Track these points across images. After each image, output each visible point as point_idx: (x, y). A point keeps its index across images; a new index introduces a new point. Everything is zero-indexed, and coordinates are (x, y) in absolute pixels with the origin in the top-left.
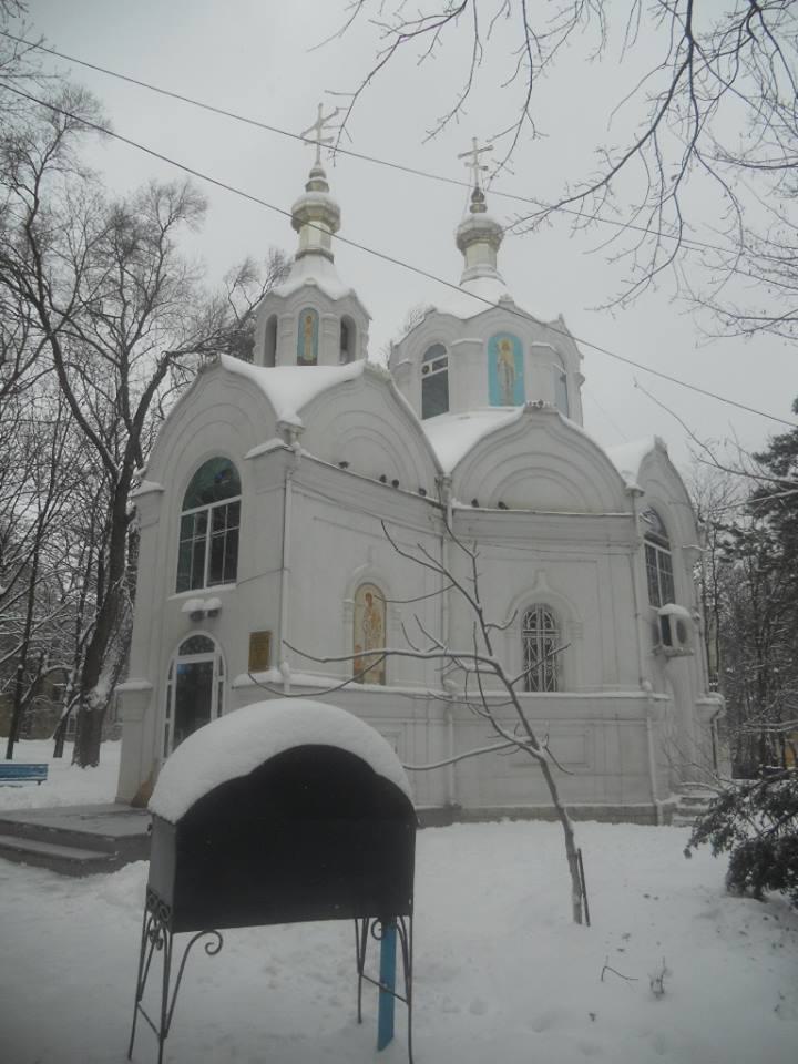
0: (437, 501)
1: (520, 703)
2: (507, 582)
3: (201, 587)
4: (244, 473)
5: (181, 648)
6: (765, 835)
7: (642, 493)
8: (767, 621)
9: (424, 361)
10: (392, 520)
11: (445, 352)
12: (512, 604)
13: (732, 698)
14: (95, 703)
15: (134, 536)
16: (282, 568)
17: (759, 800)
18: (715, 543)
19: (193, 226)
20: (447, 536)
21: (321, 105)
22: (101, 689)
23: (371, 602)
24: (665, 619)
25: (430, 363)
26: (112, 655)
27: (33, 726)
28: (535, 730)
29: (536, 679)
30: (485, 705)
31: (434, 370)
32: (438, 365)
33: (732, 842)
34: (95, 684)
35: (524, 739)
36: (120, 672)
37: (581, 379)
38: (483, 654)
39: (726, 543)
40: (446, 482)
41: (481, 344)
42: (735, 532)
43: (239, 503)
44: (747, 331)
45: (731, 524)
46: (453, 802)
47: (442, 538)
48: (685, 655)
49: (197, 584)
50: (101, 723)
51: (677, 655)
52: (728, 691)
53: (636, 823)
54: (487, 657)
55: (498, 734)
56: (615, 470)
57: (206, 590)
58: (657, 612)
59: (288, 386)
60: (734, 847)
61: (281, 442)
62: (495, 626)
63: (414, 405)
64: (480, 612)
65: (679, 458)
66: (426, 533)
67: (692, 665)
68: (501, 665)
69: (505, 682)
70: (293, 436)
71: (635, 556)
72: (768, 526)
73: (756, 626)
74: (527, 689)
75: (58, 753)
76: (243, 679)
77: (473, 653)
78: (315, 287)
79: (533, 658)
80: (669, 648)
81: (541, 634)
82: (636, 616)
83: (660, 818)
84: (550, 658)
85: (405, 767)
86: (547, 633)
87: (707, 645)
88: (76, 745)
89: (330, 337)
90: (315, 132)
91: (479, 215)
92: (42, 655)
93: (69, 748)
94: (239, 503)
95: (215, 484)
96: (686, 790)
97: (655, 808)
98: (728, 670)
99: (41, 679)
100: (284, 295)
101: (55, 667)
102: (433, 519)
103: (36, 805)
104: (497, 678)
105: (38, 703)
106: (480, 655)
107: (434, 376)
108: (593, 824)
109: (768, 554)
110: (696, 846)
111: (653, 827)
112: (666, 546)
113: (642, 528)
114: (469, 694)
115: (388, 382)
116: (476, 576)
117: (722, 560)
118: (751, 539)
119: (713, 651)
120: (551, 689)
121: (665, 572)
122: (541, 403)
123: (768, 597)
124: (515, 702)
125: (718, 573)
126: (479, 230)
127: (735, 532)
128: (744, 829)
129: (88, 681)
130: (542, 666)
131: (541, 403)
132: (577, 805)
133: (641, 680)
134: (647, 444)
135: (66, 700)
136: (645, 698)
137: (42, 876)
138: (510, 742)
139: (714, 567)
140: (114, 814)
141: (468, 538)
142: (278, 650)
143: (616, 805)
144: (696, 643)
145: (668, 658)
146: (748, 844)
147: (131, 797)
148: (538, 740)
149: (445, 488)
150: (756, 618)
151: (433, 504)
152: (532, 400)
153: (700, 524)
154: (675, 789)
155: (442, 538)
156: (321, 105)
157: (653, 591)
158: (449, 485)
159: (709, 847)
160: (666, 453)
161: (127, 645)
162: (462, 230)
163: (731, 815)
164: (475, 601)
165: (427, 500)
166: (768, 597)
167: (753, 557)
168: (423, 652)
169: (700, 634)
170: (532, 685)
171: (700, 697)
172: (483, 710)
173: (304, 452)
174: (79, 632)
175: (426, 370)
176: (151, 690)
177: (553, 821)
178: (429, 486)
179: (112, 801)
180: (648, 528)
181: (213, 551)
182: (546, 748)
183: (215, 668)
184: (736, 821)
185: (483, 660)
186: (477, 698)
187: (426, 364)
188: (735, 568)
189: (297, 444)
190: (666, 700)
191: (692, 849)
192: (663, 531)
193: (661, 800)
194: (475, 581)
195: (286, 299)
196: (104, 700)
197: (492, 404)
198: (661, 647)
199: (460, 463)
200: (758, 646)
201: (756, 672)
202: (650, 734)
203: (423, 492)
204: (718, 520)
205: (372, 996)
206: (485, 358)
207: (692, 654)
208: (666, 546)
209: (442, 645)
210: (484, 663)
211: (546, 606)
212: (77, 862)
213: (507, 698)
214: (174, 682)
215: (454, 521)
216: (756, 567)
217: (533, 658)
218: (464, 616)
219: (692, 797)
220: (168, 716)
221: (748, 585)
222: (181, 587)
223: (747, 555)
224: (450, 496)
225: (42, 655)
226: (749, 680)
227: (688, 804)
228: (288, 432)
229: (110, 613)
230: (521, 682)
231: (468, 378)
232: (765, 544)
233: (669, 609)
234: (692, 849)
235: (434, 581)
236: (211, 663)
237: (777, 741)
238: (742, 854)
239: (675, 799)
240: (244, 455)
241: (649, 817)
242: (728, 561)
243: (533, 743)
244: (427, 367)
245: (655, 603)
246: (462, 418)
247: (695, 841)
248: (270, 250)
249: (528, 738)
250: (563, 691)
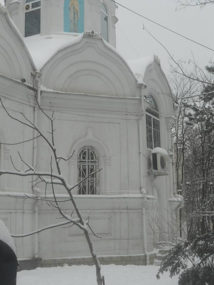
0: (32, 86)
1: (75, 200)
2: (69, 134)
6: (196, 266)
7: (146, 87)
8: (208, 157)
9: (26, 2)
10: (5, 96)
12: (72, 147)
13: (188, 198)
17: (193, 248)
18: (184, 114)
20: (37, 107)
24: (155, 155)
25: (30, 4)
28: (82, 215)
29: (85, 187)
30: (56, 202)
31: (32, 8)
33: (179, 270)
35: (76, 219)
37: (116, 20)
38: (55, 173)
39: (190, 115)
40: (37, 75)
42: (195, 109)
44: (201, 4)
45: (193, 104)
46: (37, 256)
47: (34, 107)
48: (164, 175)
51: (160, 175)
52: (187, 194)
53: (135, 264)
54: (58, 175)
55: (62, 216)
56: (131, 73)
58: (151, 151)
60: (180, 273)
62: (62, 159)
63: (20, 29)
64: (54, 151)
65: (166, 68)
66: (26, 104)
67: (168, 180)
68: (65, 180)
69: (67, 189)
71: (140, 121)
72: (211, 106)
73: (203, 159)
74: (80, 193)
77: (50, 173)
79: (83, 176)
80: (156, 171)
81: (89, 165)
83: (148, 262)
84: (93, 176)
85: (12, 236)
86: (91, 162)
87: (177, 170)
96: (161, 246)
97: (146, 256)
98: (187, 183)
102: (30, 96)
104: (63, 186)
106: (53, 174)
107: (33, 11)
108: (112, 266)
109: (211, 121)
110: (162, 272)
111: (144, 266)
112: (157, 115)
113: (145, 106)
114: (47, 196)
115: (5, 14)
116: (53, 131)
117: (187, 123)
118: (202, 113)
119: (180, 172)
120: (93, 193)
121: (154, 129)
122: (93, 32)
123: (209, 144)
124: (72, 199)
125: (185, 131)
127: (195, 109)
128: (186, 263)
130: (88, 181)
131: (93, 32)
132: (104, 256)
133: (141, 188)
134: (149, 59)
136: (143, 198)
138: (69, 221)
139: (183, 127)
141: (50, 108)
143: (125, 256)
144: (171, 169)
145: (155, 176)
146: (188, 271)
148: (83, 220)
149: (37, 78)
150: (203, 156)
151: (29, 88)
152: (88, 30)
153: (176, 104)
154: (156, 245)
155: (34, 107)
157: (149, 139)
158: (39, 77)
159: (168, 273)
160: (159, 65)
163: (180, 257)
164: (52, 144)
166: (209, 144)
167: (203, 123)
168: (22, 172)
169: (173, 164)
170: (82, 191)
171: (171, 197)
172: (54, 203)
175: (27, 7)
177: (92, 265)
178: (27, 76)
180: (148, 106)
182: (87, 224)
184: (182, 260)
185: (56, 177)
186: (52, 198)
187: (27, 4)
188: (194, 128)
190: (153, 199)
191: (160, 274)
192: (156, 108)
193: (149, 252)
194: (52, 134)
197: (65, 31)
198: (152, 170)
199: (45, 65)
200: (203, 170)
201: (202, 184)
202: (144, 217)
203: (24, 81)
204: (186, 102)
207: (167, 174)
209: (33, 168)
210: (56, 178)
211: (92, 147)
213: (68, 198)
215: (42, 98)
216: (205, 127)
217: (83, 176)
218: (46, 153)
219: (164, 250)
221: (200, 138)
223: (200, 121)
224: (39, 83)
226: (198, 189)
227: (162, 254)
230: (77, 189)
232: (210, 116)
233: (157, 150)
234: (160, 274)
235: (29, 132)
237: (210, 221)
238: (185, 276)
239: (156, 251)
241: (142, 261)
242: (190, 124)
243: (81, 221)
245: (150, 146)
246: (48, 38)
247: (161, 271)
249: (78, 219)
250: (99, 194)
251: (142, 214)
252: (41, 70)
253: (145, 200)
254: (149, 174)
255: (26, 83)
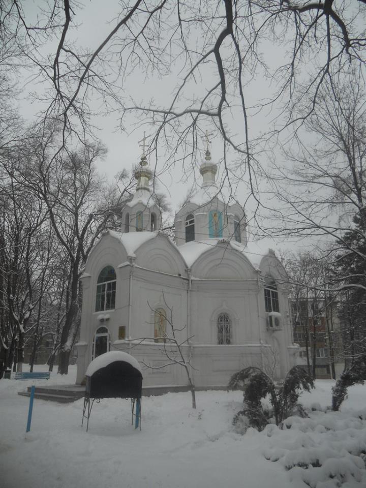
3: (103, 310)
4: (117, 271)
5: (97, 331)
9: (186, 220)
11: (193, 217)
14: (66, 349)
15: (80, 282)
16: (129, 305)
19: (102, 159)
21: (145, 132)
22: (69, 343)
23: (161, 317)
24: (271, 317)
25: (188, 221)
26: (72, 331)
27: (38, 358)
32: (191, 222)
34: (66, 341)
36: (76, 335)
41: (206, 215)
43: (116, 282)
47: (316, 217)
49: (102, 309)
50: (69, 357)
51: (276, 330)
57: (105, 311)
58: (268, 314)
59: (132, 241)
61: (128, 263)
68: (177, 341)
70: (133, 261)
74: (219, 344)
75: (51, 369)
76: (117, 342)
78: (142, 203)
82: (259, 316)
88: (215, 53)
89: (147, 219)
90: (143, 142)
91: (208, 161)
92: (43, 327)
93: (56, 368)
94: (116, 282)
95: (108, 274)
99: (42, 338)
100: (131, 206)
101: (49, 333)
103: (49, 385)
105: (40, 349)
120: (228, 344)
126: (208, 167)
129: (64, 341)
133: (260, 340)
135: (54, 348)
136: (260, 346)
137: (55, 403)
140: (76, 387)
142: (130, 332)
147: (80, 382)
149: (189, 273)
151: (184, 279)
156: (145, 132)
158: (190, 271)
161: (78, 325)
162: (202, 167)
165: (181, 278)
173: (136, 266)
174: (58, 319)
175: (187, 224)
176: (87, 345)
178: (182, 272)
179: (74, 383)
181: (107, 298)
183: (108, 338)
189: (134, 263)
195: (132, 208)
196: (70, 348)
199: (194, 263)
203: (180, 275)
205: (135, 417)
206: (207, 220)
208: (276, 289)
212: (66, 399)
214: (95, 343)
220: (93, 354)
222: (97, 310)
224: (190, 276)
225: (43, 327)
228: (131, 259)
229: (72, 313)
231: (201, 227)
236: (107, 336)
240: (118, 266)
244: (187, 223)
245: (268, 309)
248: (133, 165)
251: (262, 358)
252: (191, 267)
253: (263, 348)
254: (267, 330)
255: (182, 277)
